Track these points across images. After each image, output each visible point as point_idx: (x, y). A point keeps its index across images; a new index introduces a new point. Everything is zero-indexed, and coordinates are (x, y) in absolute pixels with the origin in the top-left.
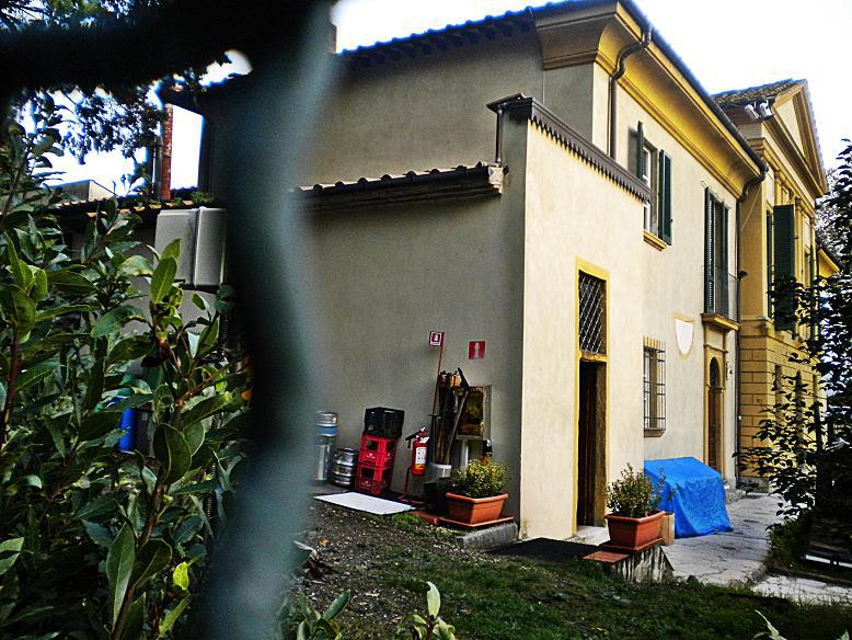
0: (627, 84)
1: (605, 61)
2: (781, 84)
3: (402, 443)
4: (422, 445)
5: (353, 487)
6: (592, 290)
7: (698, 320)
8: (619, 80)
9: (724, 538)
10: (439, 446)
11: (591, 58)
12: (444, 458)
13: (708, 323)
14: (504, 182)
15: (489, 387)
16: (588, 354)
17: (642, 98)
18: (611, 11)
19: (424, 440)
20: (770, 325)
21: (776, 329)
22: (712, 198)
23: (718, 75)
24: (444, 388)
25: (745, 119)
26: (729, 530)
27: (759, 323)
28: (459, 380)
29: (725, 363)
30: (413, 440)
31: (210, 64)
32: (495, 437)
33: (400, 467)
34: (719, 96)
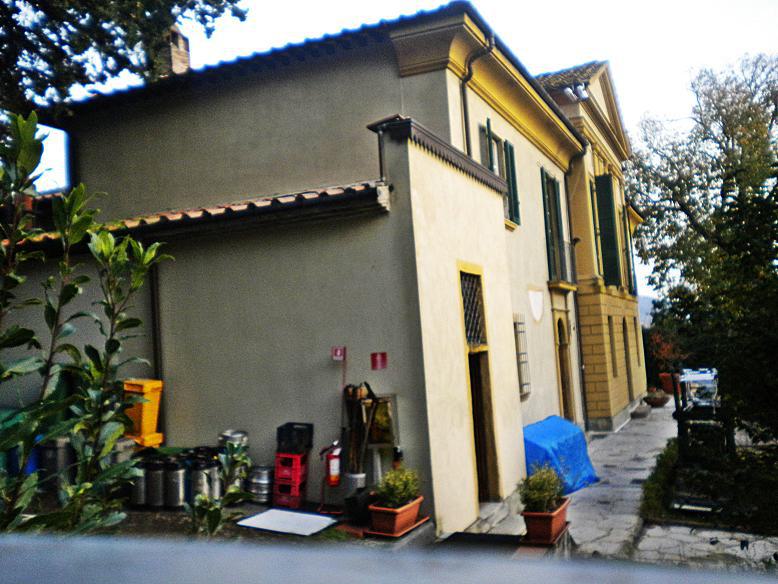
0: (475, 85)
1: (456, 68)
2: (589, 66)
3: (315, 455)
4: (335, 457)
5: (271, 504)
6: (471, 284)
7: (545, 287)
8: (469, 82)
9: (594, 491)
10: (351, 456)
11: (444, 65)
12: (358, 467)
13: (554, 289)
14: (391, 200)
15: (394, 396)
16: (474, 347)
17: (488, 96)
18: (460, 21)
19: (337, 452)
20: (601, 282)
21: (606, 285)
22: (547, 175)
23: (540, 58)
24: (351, 399)
25: (566, 101)
26: (597, 480)
27: (592, 282)
28: (364, 391)
29: (568, 322)
30: (325, 454)
31: (70, 86)
32: (404, 442)
33: (316, 478)
34: (537, 77)
